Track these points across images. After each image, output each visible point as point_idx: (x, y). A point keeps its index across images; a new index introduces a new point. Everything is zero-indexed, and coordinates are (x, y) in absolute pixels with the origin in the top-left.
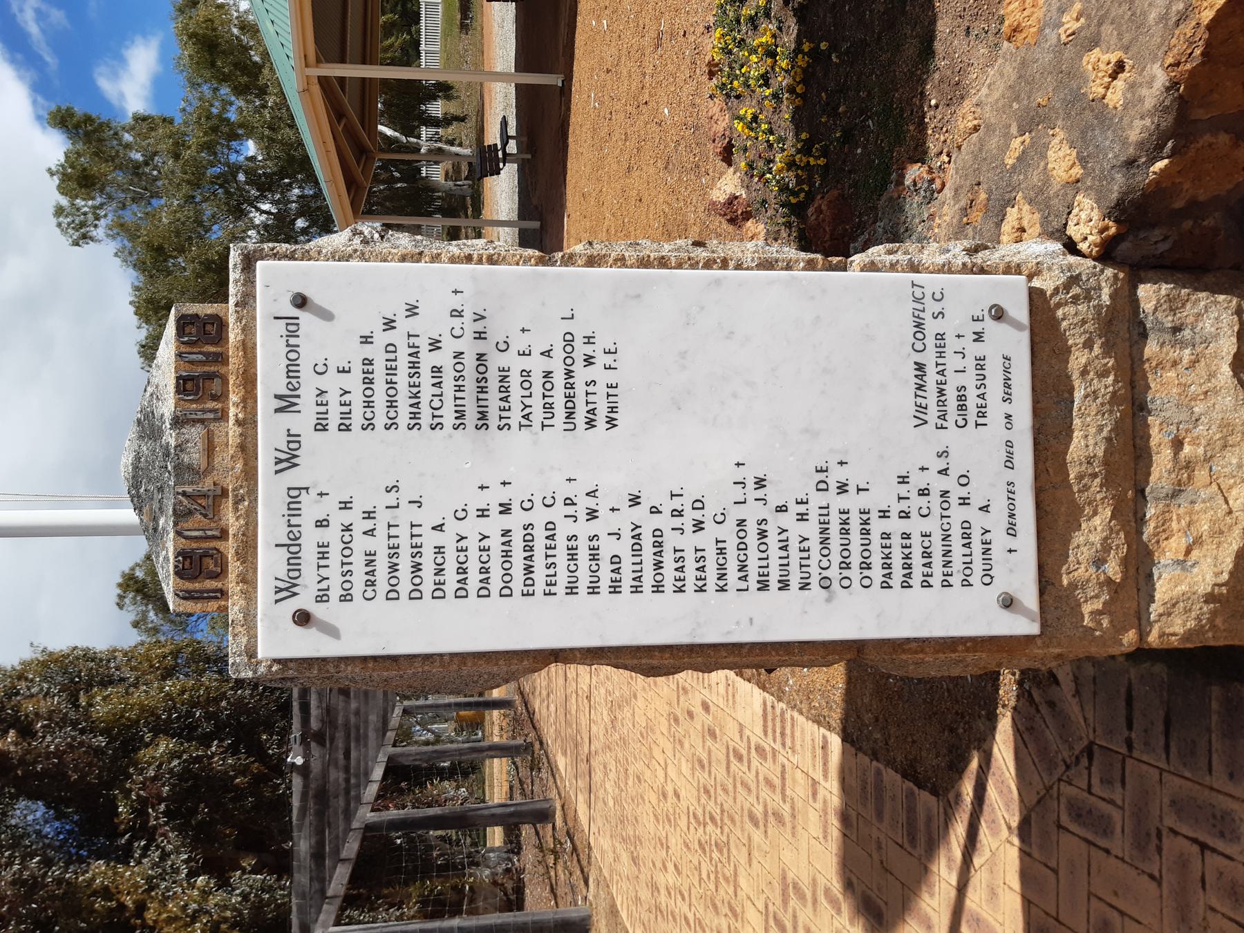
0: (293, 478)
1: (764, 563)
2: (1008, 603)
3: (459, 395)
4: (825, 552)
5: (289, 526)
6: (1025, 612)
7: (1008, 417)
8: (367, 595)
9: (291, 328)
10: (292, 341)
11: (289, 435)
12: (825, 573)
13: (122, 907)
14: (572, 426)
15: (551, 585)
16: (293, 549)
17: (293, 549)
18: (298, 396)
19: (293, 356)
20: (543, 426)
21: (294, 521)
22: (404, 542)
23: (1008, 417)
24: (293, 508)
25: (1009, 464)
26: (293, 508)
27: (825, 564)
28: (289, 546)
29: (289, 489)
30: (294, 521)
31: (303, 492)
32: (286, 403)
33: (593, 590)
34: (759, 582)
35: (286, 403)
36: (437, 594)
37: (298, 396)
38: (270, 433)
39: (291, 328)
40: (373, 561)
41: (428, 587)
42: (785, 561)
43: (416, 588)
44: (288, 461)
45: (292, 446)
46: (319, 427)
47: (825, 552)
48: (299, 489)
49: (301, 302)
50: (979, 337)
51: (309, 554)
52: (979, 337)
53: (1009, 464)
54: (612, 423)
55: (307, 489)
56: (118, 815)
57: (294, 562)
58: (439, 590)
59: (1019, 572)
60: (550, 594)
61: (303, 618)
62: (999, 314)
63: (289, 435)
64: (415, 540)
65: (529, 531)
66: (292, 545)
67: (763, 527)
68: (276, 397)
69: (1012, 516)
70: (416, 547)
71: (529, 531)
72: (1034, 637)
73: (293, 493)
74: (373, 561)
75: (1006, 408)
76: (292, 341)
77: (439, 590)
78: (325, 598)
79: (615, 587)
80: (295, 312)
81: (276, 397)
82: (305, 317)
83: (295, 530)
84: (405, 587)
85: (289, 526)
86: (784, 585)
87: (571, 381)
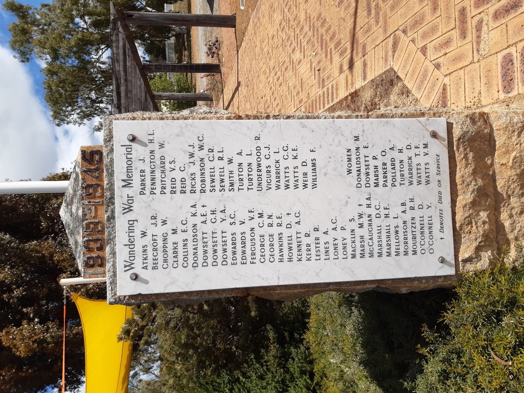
0: (130, 216)
1: (398, 244)
2: (443, 261)
3: (231, 175)
4: (423, 238)
5: (129, 236)
6: (450, 265)
7: (439, 181)
8: (164, 266)
9: (128, 150)
10: (129, 156)
11: (128, 197)
12: (431, 247)
13: (44, 255)
14: (261, 189)
15: (253, 259)
16: (131, 247)
17: (131, 247)
18: (132, 180)
19: (129, 163)
20: (239, 189)
21: (131, 234)
22: (219, 240)
23: (439, 181)
24: (131, 229)
25: (440, 201)
26: (131, 229)
27: (423, 243)
28: (130, 245)
29: (129, 221)
30: (131, 234)
31: (135, 222)
32: (127, 184)
33: (371, 255)
34: (352, 254)
35: (127, 184)
36: (214, 264)
37: (132, 180)
38: (121, 196)
39: (128, 150)
40: (300, 245)
41: (220, 260)
42: (186, 254)
43: (225, 260)
44: (128, 209)
45: (130, 202)
46: (172, 192)
47: (423, 238)
48: (134, 221)
49: (134, 139)
50: (426, 146)
51: (138, 249)
52: (426, 146)
53: (440, 201)
54: (314, 186)
55: (137, 221)
56: (41, 225)
57: (132, 254)
58: (224, 262)
59: (446, 248)
60: (253, 263)
61: (136, 277)
62: (434, 135)
63: (128, 197)
64: (224, 239)
65: (243, 235)
66: (131, 243)
67: (397, 229)
68: (123, 180)
69: (442, 224)
70: (224, 242)
71: (243, 235)
72: (452, 276)
73: (130, 223)
74: (300, 245)
75: (438, 177)
76: (129, 156)
77: (224, 262)
78: (156, 268)
79: (290, 259)
80: (131, 143)
81: (123, 180)
82: (134, 145)
83: (132, 238)
84: (210, 261)
85: (129, 236)
86: (363, 256)
87: (260, 168)
